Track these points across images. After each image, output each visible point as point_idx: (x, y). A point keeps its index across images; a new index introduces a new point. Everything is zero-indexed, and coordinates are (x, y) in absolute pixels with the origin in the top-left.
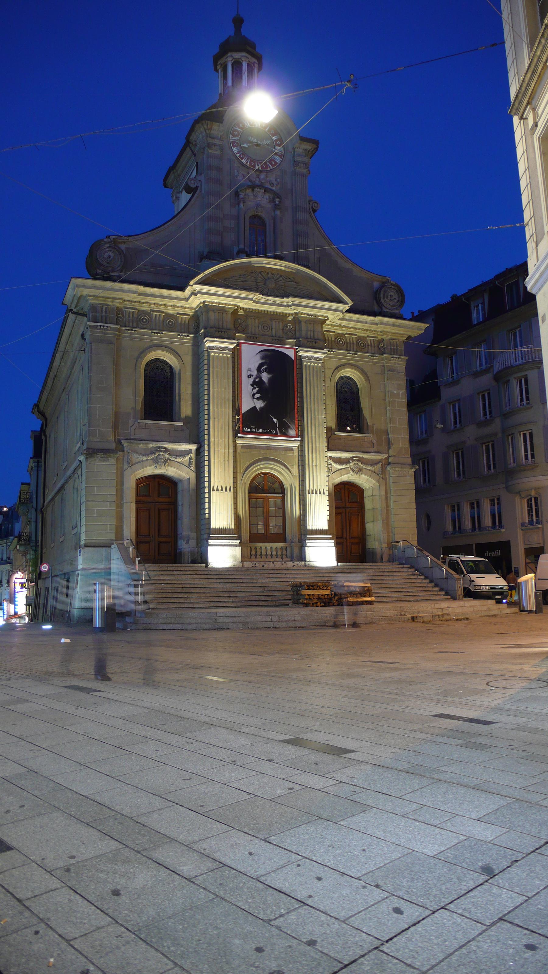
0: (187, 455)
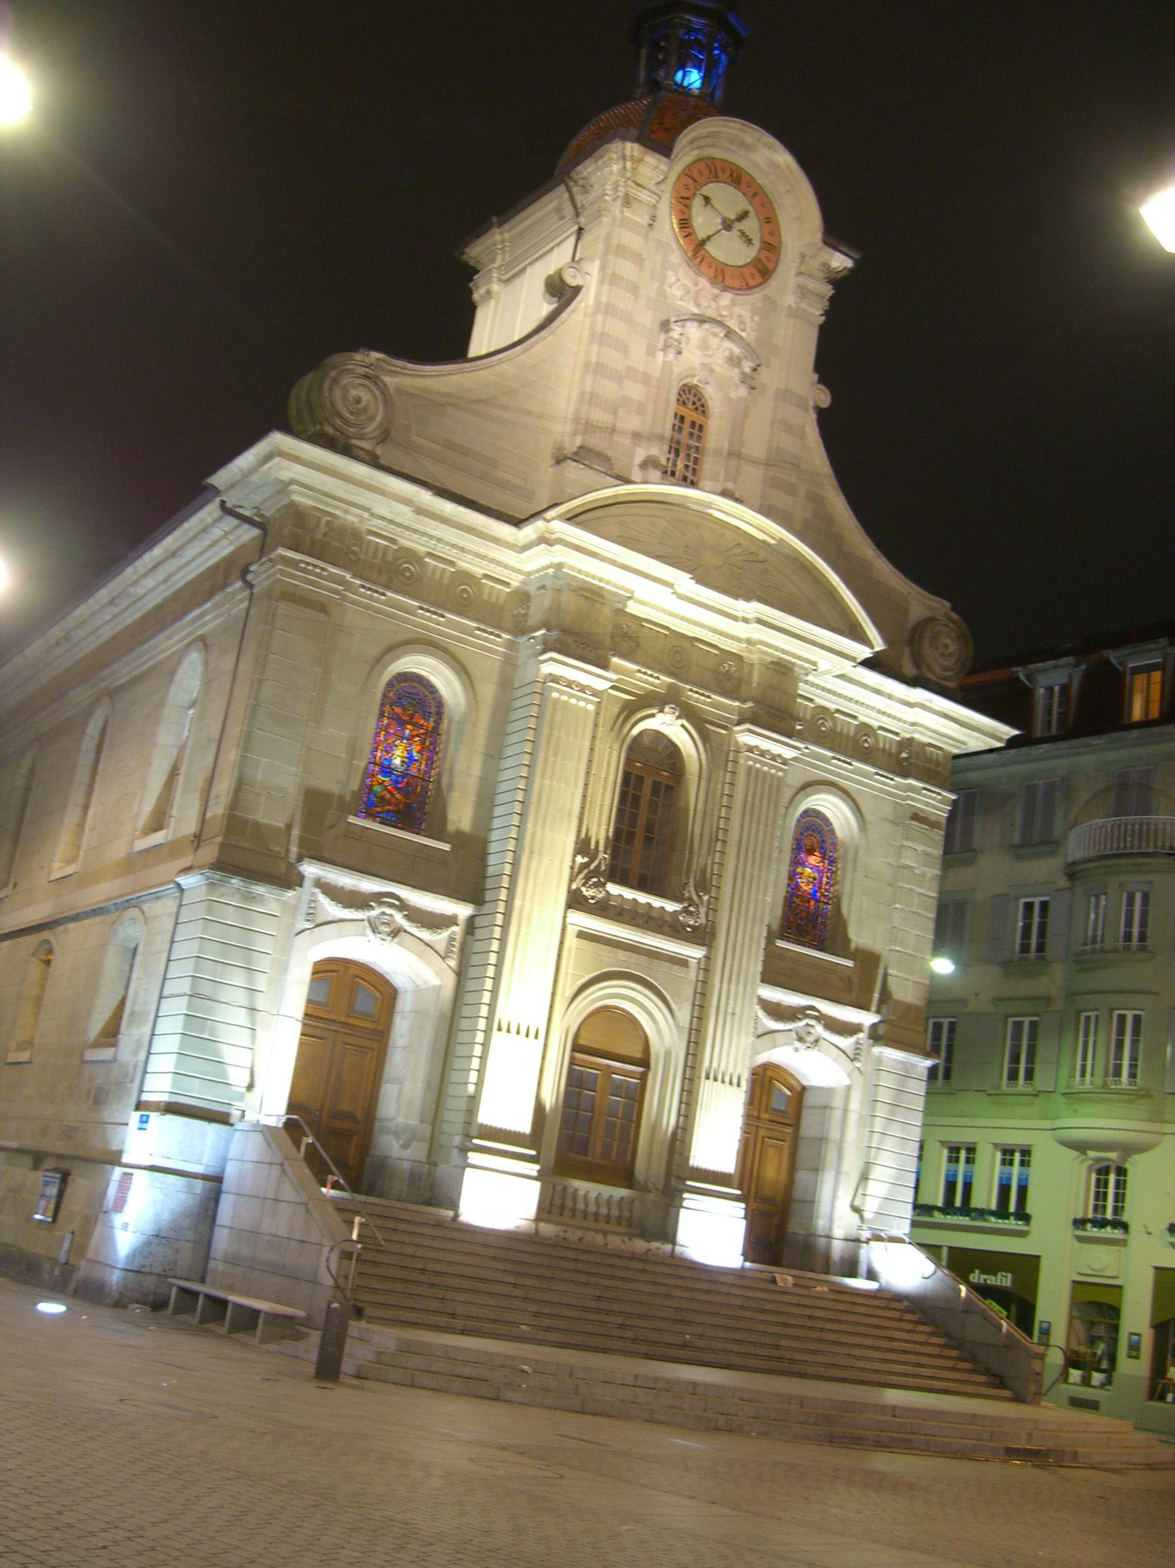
0: (448, 926)
